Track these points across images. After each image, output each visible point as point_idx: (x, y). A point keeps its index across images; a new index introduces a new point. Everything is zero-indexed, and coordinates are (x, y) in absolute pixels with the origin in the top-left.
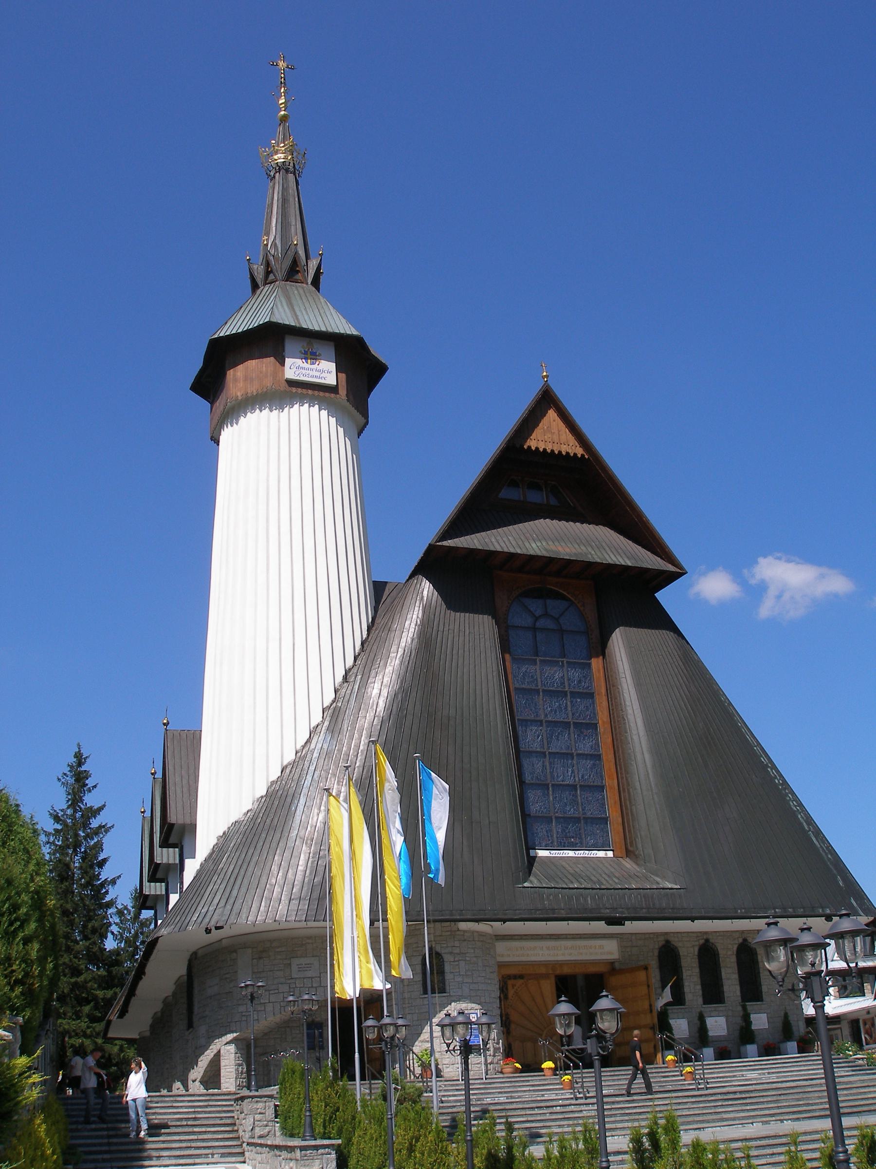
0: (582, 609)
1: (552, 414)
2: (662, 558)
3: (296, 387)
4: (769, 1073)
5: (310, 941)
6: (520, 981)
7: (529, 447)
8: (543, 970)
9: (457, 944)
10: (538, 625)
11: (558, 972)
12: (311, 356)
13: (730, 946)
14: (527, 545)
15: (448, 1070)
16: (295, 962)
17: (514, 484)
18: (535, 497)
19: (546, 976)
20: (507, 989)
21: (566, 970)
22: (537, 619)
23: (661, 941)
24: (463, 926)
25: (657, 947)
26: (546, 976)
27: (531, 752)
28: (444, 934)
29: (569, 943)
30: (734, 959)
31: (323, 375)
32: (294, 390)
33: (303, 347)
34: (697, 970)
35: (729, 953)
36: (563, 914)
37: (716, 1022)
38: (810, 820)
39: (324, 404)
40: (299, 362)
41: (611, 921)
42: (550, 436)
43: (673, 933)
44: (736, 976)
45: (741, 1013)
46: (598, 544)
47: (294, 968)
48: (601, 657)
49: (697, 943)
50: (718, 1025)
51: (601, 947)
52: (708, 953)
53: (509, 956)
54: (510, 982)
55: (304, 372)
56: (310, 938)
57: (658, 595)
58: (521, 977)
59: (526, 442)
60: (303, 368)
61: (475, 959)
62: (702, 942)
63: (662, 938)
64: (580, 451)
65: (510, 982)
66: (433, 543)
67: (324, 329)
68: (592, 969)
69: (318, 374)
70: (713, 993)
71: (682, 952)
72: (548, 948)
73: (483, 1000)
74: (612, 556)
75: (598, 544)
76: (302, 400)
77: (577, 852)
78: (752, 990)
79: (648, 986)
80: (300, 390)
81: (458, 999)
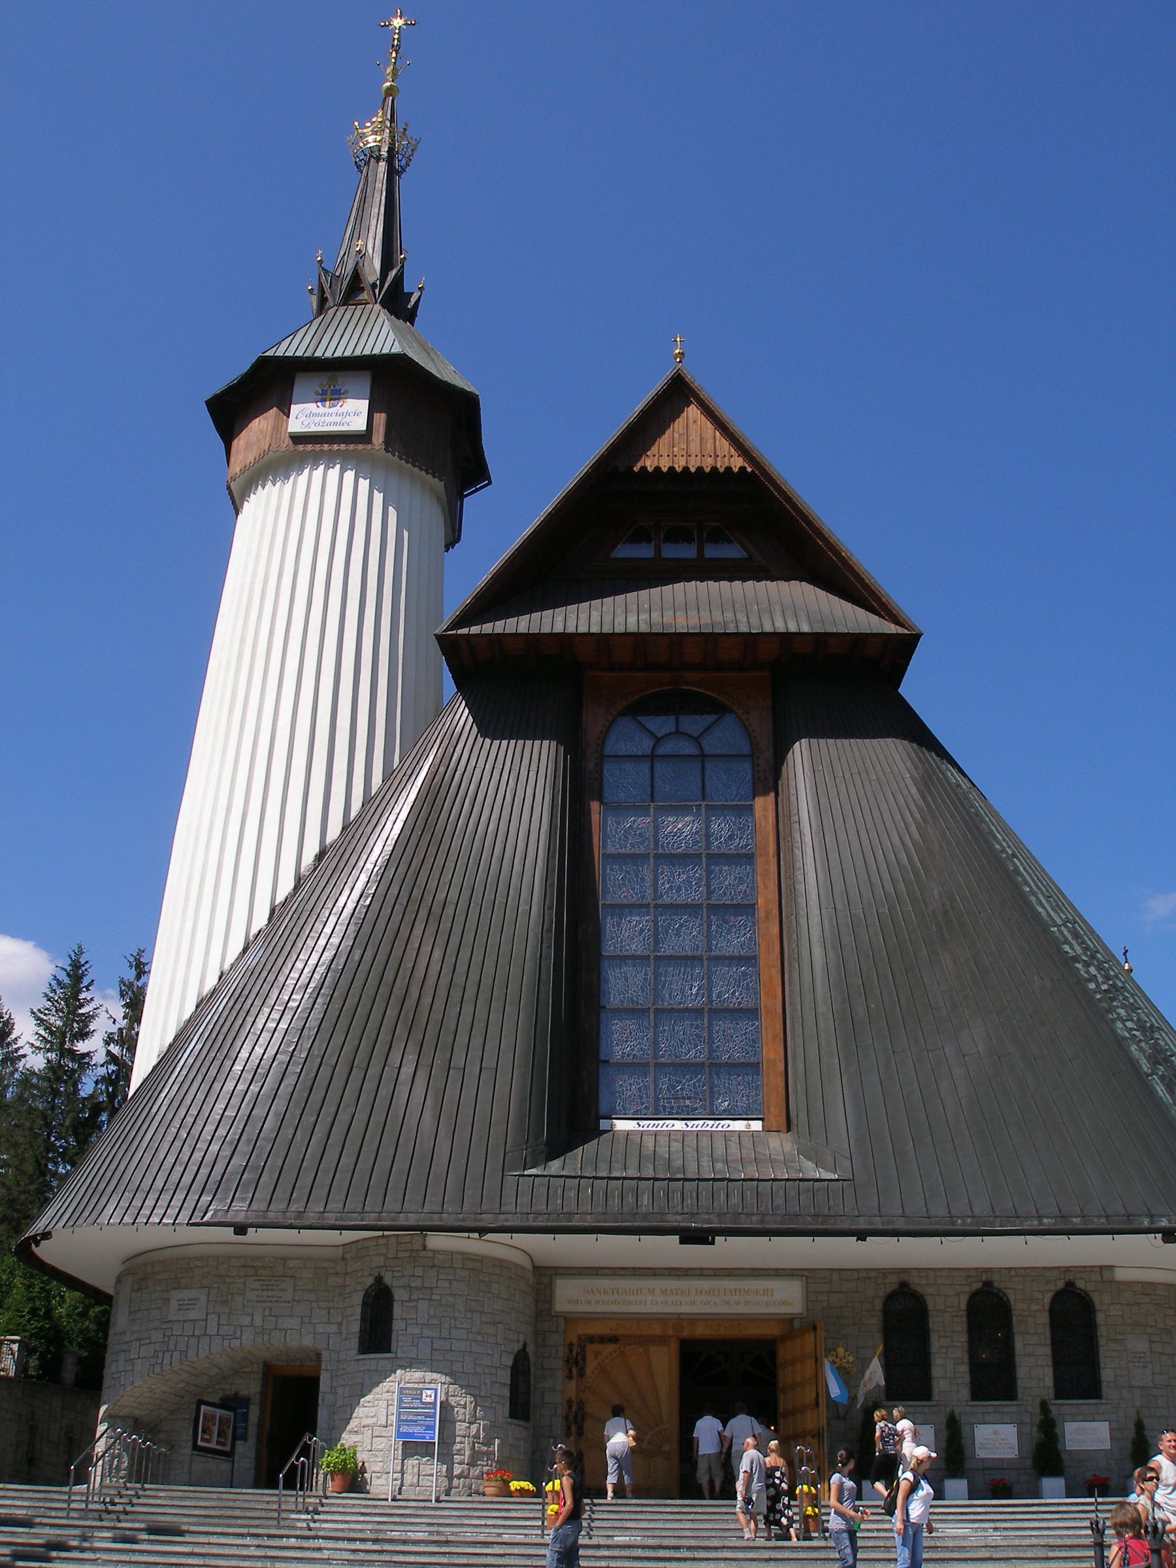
0: (744, 717)
1: (693, 411)
2: (881, 616)
3: (314, 443)
4: (995, 1529)
6: (611, 1347)
7: (644, 468)
8: (657, 1330)
9: (419, 1271)
10: (661, 751)
11: (686, 1333)
12: (332, 395)
13: (1037, 1295)
15: (379, 1482)
16: (176, 1296)
17: (640, 536)
18: (732, 551)
19: (662, 1340)
20: (584, 1359)
21: (701, 1331)
22: (658, 740)
23: (892, 1283)
24: (437, 1241)
25: (882, 1294)
26: (662, 1340)
27: (623, 959)
28: (401, 1255)
29: (705, 1284)
30: (1044, 1319)
31: (348, 419)
32: (301, 447)
33: (321, 385)
34: (964, 1338)
35: (1034, 1307)
37: (996, 1433)
39: (346, 461)
40: (311, 407)
41: (691, 1237)
42: (688, 445)
44: (1047, 1350)
45: (1039, 1418)
46: (789, 607)
47: (174, 1304)
48: (772, 795)
49: (967, 1289)
50: (997, 1439)
51: (766, 1291)
52: (988, 1306)
53: (589, 1302)
54: (590, 1348)
55: (317, 419)
56: (197, 1258)
58: (614, 1339)
59: (638, 460)
60: (318, 415)
61: (451, 1299)
62: (977, 1286)
63: (893, 1279)
64: (737, 463)
65: (590, 1348)
68: (754, 1331)
69: (338, 419)
70: (994, 1381)
71: (933, 1304)
72: (664, 1292)
73: (457, 1367)
75: (789, 607)
76: (314, 460)
77: (690, 1123)
78: (1079, 1377)
79: (816, 1361)
80: (309, 447)
81: (410, 1364)
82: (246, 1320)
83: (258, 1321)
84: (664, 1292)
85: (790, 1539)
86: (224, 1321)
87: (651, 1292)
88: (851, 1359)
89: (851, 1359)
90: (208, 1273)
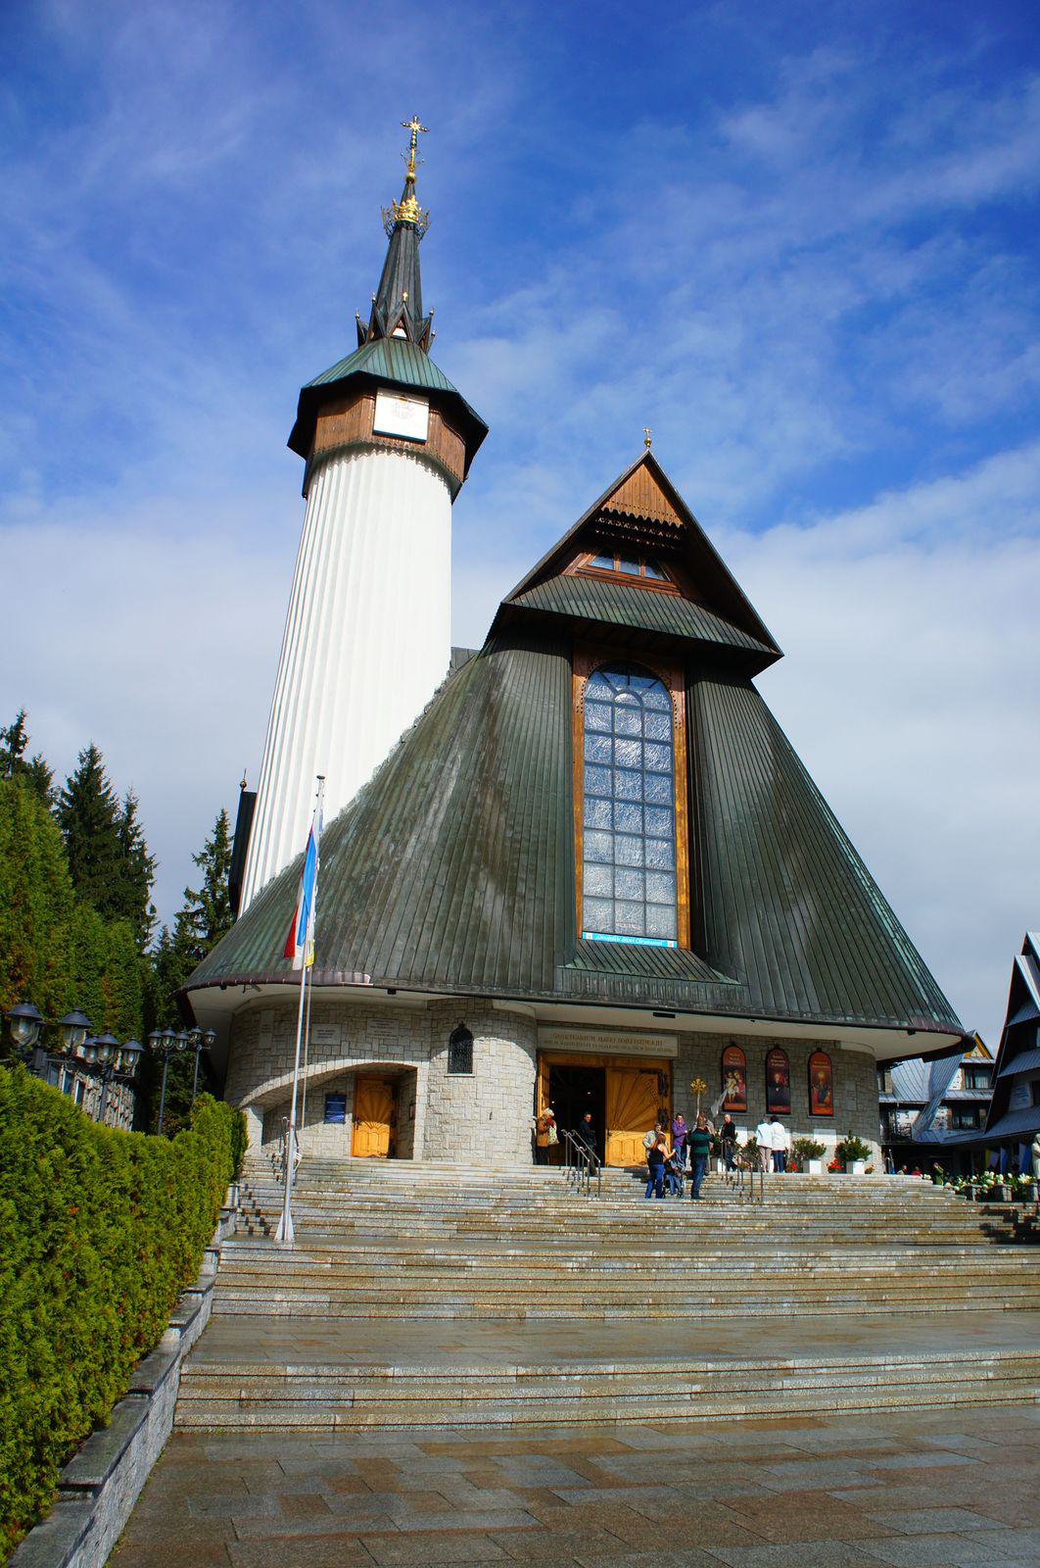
5: (333, 1007)
7: (606, 509)
14: (565, 603)
29: (604, 1034)
36: (606, 1000)
38: (898, 928)
41: (660, 1013)
43: (741, 1035)
46: (708, 628)
51: (658, 1043)
57: (755, 680)
66: (507, 601)
67: (418, 382)
72: (601, 1039)
74: (703, 632)
82: (367, 1047)
83: (376, 1048)
84: (601, 1039)
85: (1000, 1199)
86: (353, 1046)
87: (593, 1038)
88: (704, 1086)
89: (704, 1086)
90: (340, 1014)
